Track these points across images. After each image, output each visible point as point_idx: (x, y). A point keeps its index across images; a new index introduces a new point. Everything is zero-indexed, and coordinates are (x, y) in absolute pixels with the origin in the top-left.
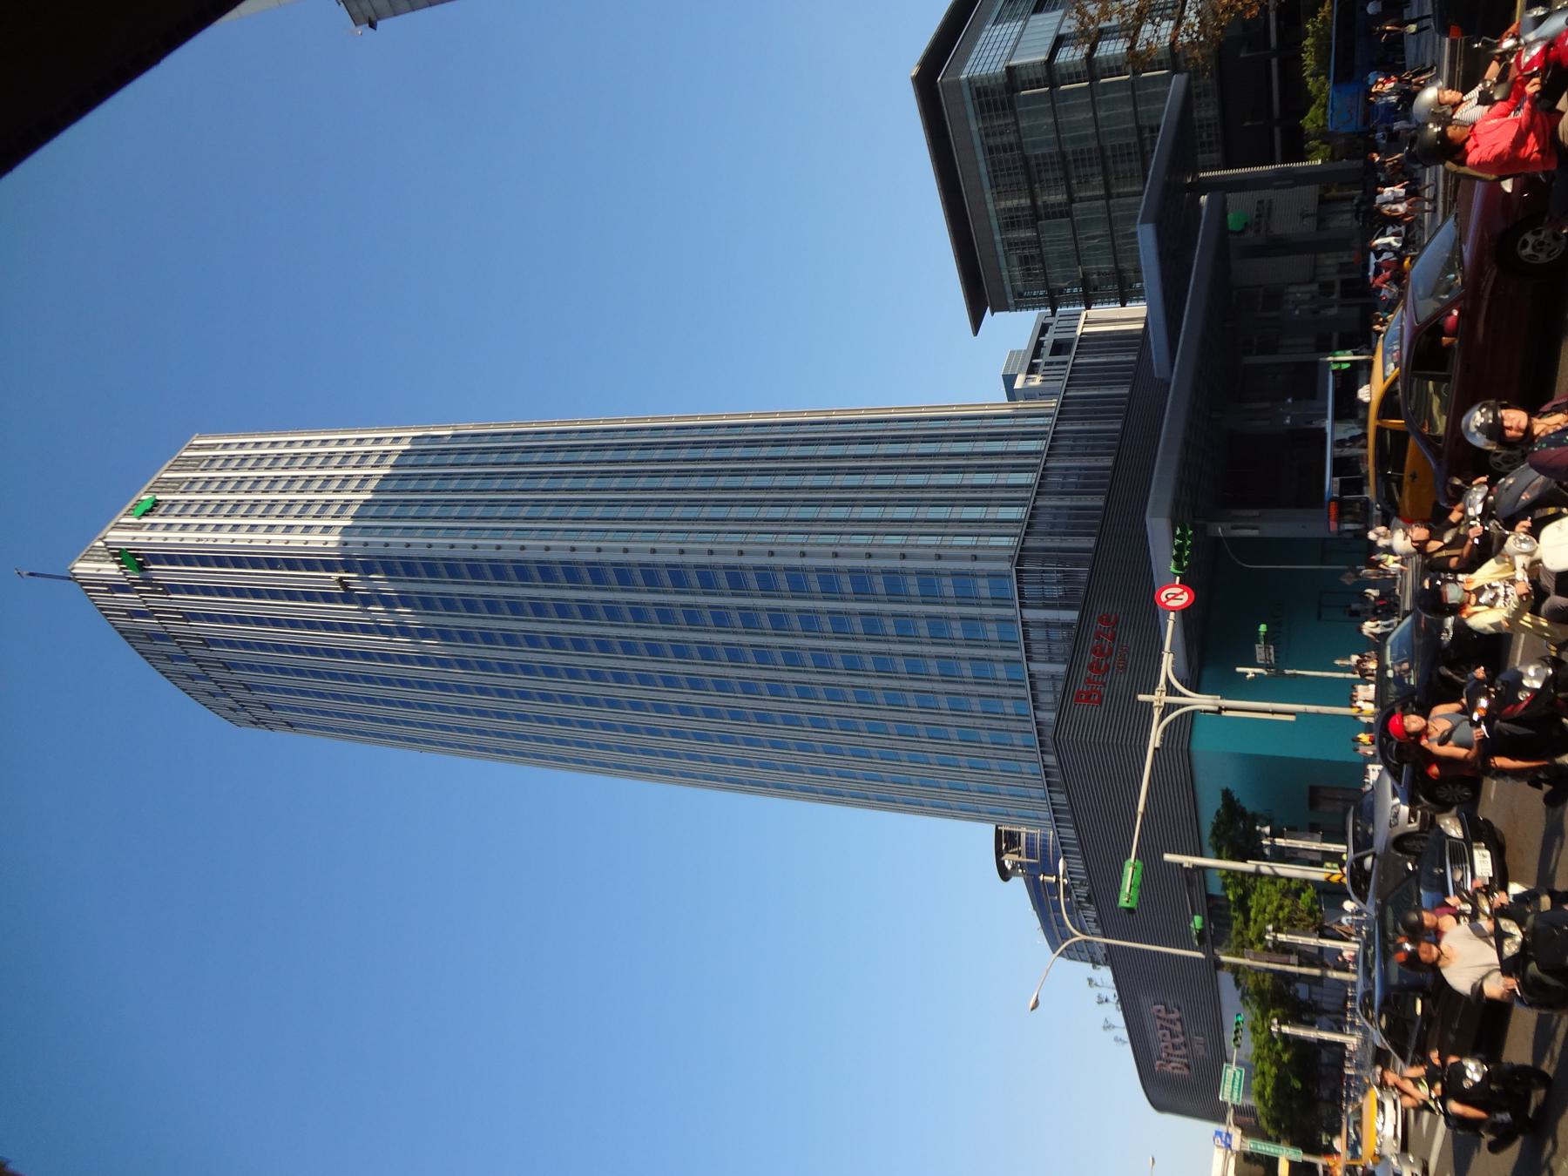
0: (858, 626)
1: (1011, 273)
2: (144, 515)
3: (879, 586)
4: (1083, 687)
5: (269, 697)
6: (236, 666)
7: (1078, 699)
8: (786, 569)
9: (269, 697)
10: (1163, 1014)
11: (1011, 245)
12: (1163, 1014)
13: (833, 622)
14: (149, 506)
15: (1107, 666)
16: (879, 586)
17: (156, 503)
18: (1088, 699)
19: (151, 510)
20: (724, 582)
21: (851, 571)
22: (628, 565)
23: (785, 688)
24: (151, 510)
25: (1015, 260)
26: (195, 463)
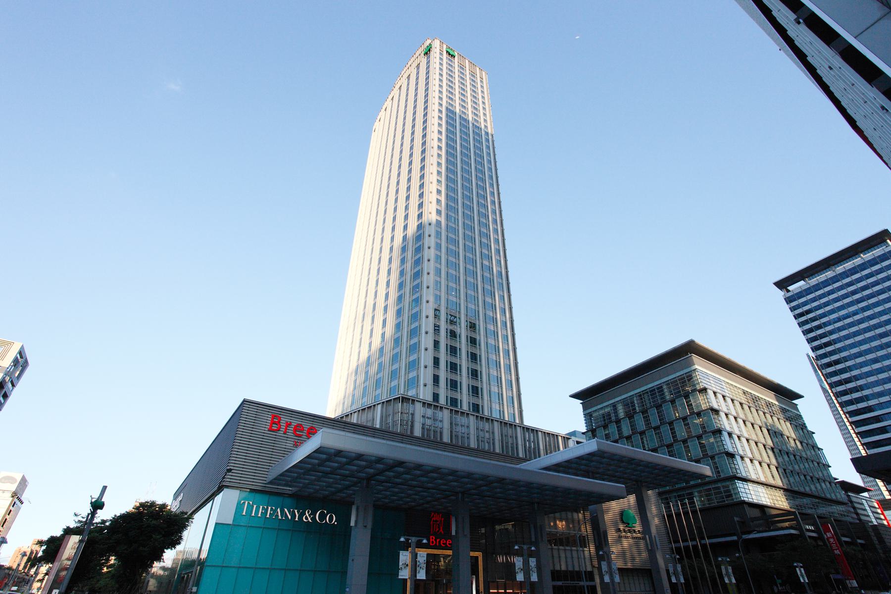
11: (614, 406)
14: (451, 53)
17: (453, 56)
18: (273, 422)
26: (473, 75)
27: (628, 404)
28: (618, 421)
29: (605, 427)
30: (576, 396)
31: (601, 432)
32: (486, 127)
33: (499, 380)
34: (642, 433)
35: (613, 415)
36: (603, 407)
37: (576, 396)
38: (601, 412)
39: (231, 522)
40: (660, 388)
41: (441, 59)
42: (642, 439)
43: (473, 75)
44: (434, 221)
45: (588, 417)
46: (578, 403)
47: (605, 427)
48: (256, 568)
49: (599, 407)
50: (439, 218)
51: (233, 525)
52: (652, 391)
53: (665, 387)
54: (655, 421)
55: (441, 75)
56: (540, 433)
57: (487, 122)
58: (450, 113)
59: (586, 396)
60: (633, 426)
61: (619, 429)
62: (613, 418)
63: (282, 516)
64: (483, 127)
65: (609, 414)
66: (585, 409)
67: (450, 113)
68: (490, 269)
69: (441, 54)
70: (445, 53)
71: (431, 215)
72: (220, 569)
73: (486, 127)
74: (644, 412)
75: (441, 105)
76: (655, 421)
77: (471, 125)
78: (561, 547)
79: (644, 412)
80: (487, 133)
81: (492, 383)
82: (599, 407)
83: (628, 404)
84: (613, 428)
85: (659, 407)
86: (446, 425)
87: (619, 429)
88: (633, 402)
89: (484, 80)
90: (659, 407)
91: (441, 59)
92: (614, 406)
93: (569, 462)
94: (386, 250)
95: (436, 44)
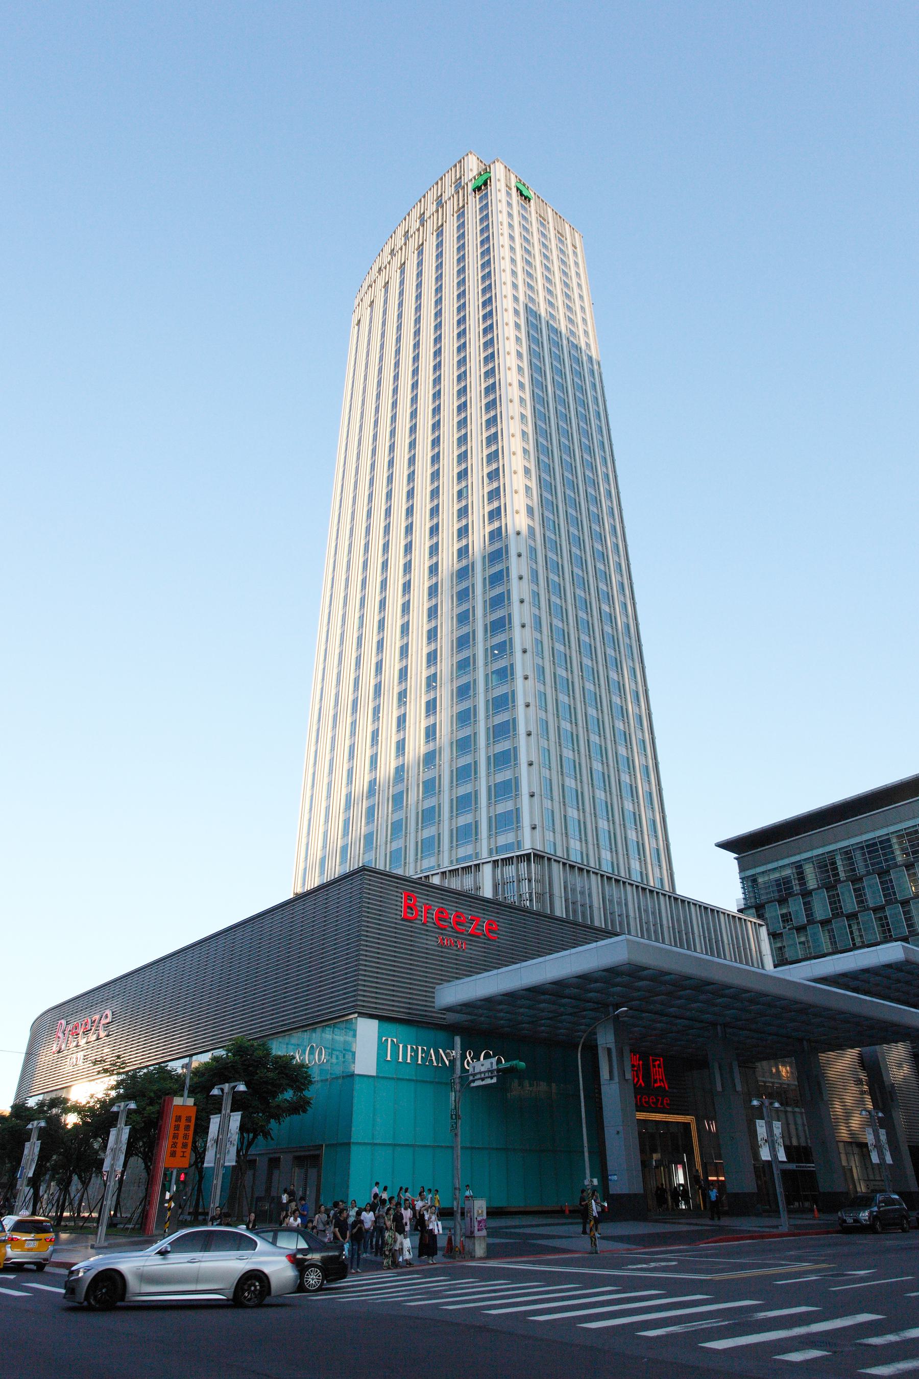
0: (465, 820)
1: (778, 866)
2: (518, 189)
3: (504, 807)
4: (421, 902)
5: (379, 303)
6: (403, 272)
7: (408, 896)
8: (517, 779)
9: (379, 303)
10: (104, 1021)
11: (799, 867)
12: (104, 1021)
13: (467, 826)
14: (525, 193)
15: (443, 928)
16: (504, 807)
17: (527, 199)
18: (408, 906)
19: (522, 195)
20: (499, 719)
21: (517, 780)
22: (509, 604)
23: (398, 838)
24: (522, 195)
25: (788, 872)
26: (561, 237)
27: (826, 865)
28: (806, 894)
29: (782, 901)
30: (727, 845)
31: (774, 911)
32: (588, 345)
33: (637, 818)
34: (852, 916)
35: (795, 883)
36: (778, 866)
37: (727, 845)
38: (776, 875)
39: (373, 1073)
40: (885, 843)
41: (509, 205)
42: (850, 926)
43: (561, 237)
44: (524, 531)
45: (750, 882)
46: (730, 859)
47: (782, 901)
48: (395, 1145)
49: (770, 866)
50: (531, 523)
51: (377, 1077)
52: (871, 848)
53: (894, 840)
54: (875, 897)
55: (512, 238)
56: (722, 916)
57: (590, 340)
58: (532, 314)
59: (744, 847)
60: (835, 903)
61: (808, 906)
62: (797, 888)
63: (438, 1063)
64: (584, 347)
65: (786, 881)
66: (742, 869)
67: (532, 314)
68: (612, 618)
69: (509, 194)
70: (514, 190)
71: (518, 518)
72: (369, 1147)
73: (588, 345)
74: (856, 880)
75: (516, 299)
76: (875, 897)
77: (565, 342)
78: (797, 1110)
79: (856, 880)
80: (590, 358)
81: (628, 825)
82: (770, 866)
83: (826, 865)
84: (796, 906)
85: (883, 873)
86: (596, 902)
87: (808, 906)
88: (834, 863)
89: (579, 250)
90: (883, 873)
91: (509, 205)
92: (799, 867)
93: (844, 975)
94: (421, 581)
95: (498, 172)
